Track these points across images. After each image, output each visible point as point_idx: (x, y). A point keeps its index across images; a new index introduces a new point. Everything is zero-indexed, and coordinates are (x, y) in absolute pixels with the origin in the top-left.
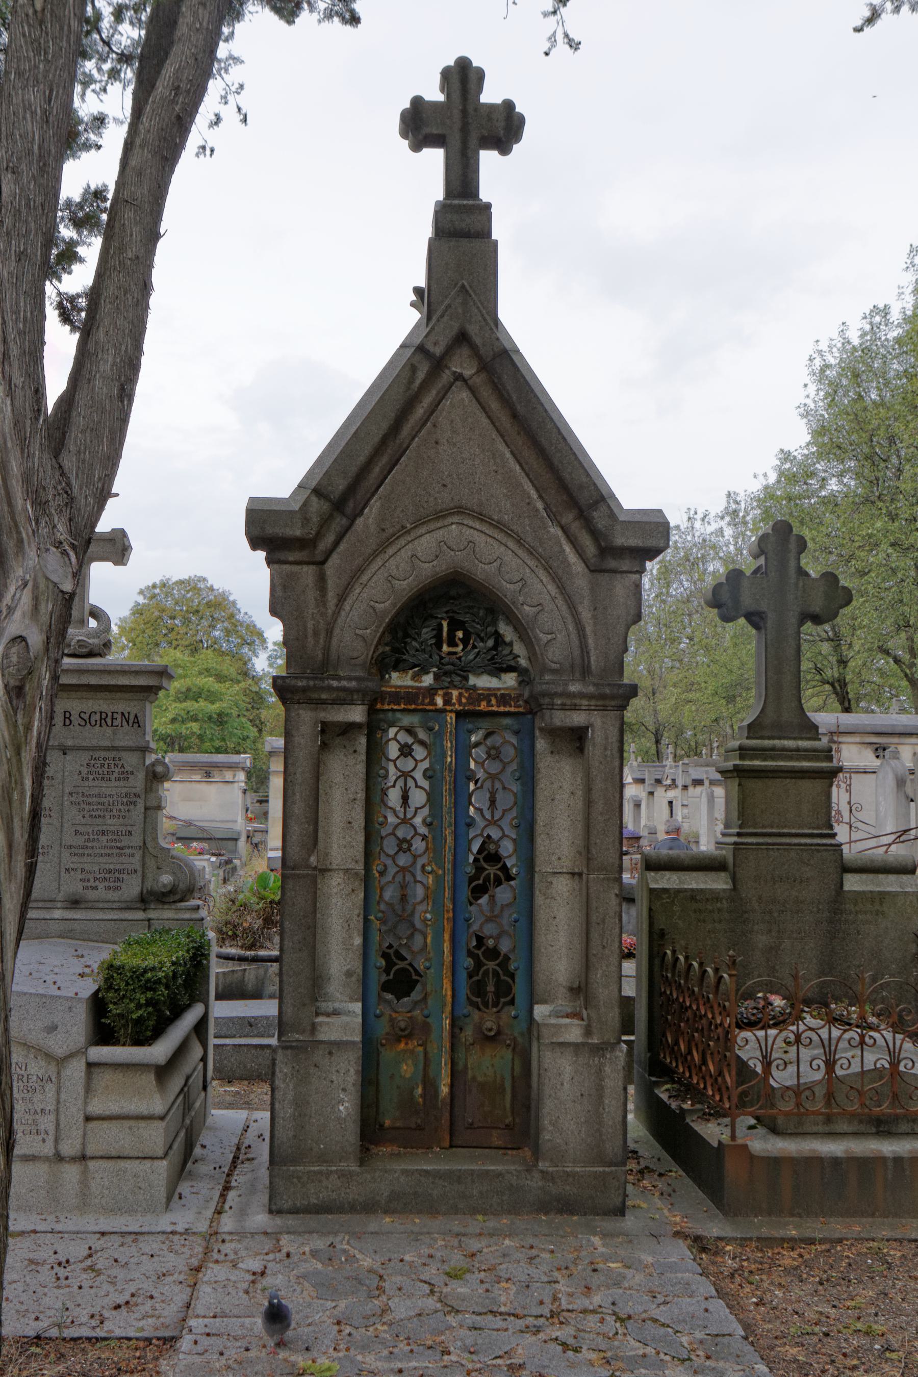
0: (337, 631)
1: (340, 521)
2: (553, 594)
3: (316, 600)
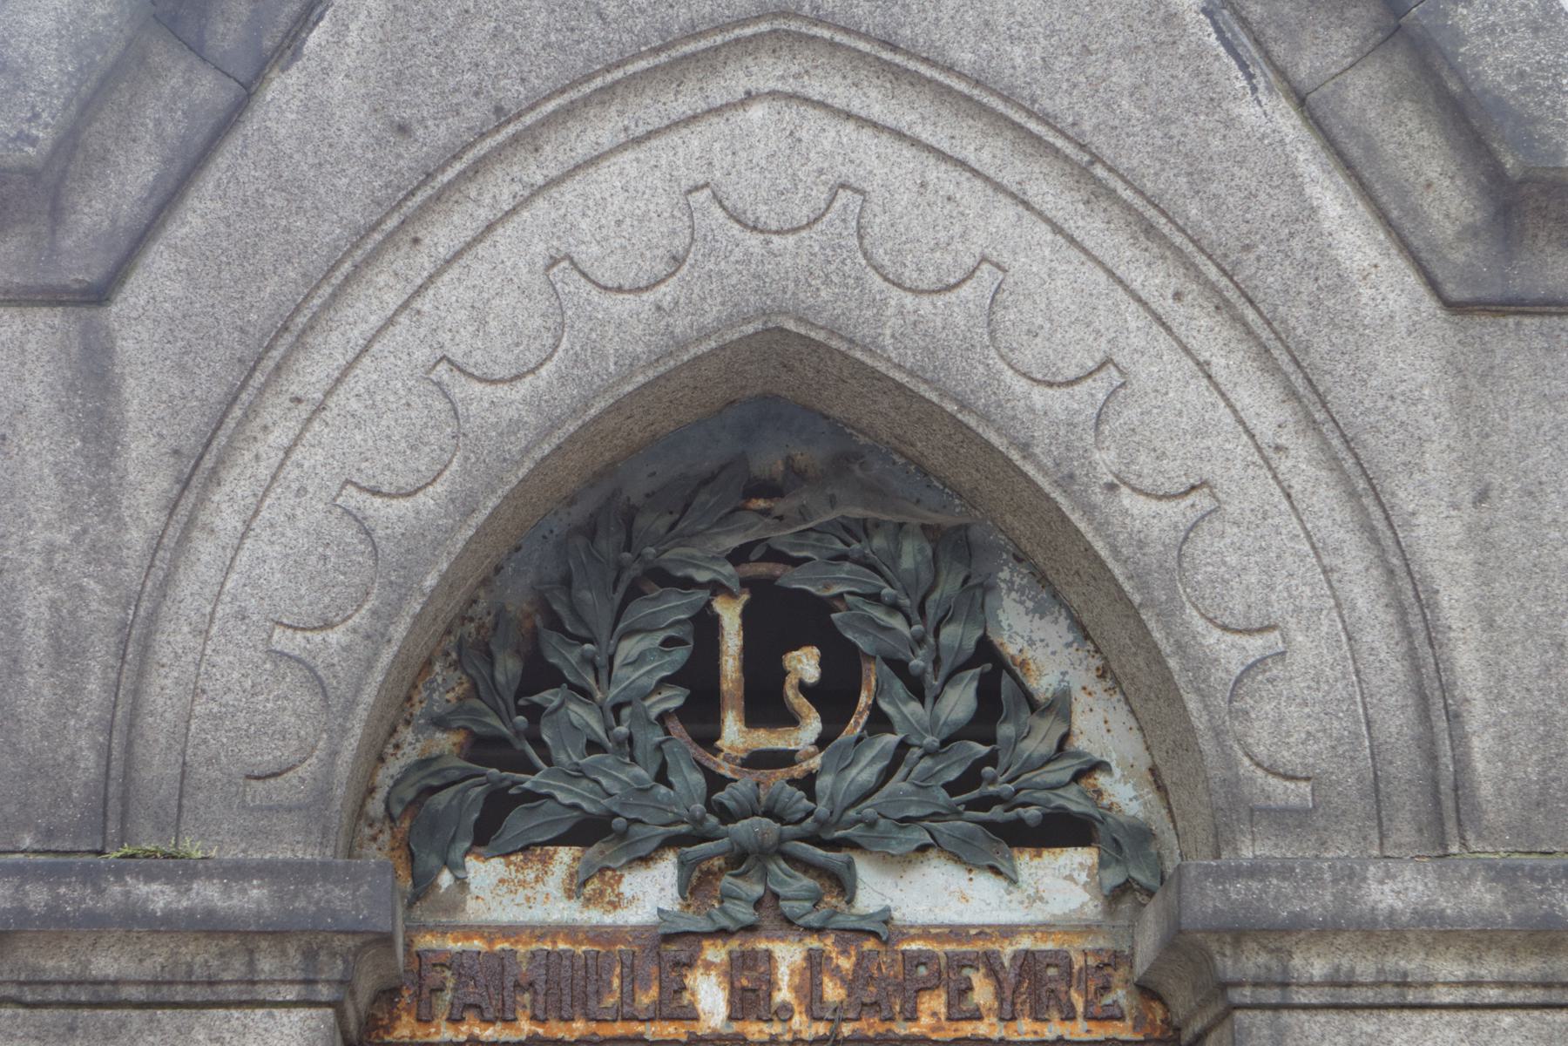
0: (174, 638)
1: (182, 91)
2: (1265, 430)
3: (64, 478)
